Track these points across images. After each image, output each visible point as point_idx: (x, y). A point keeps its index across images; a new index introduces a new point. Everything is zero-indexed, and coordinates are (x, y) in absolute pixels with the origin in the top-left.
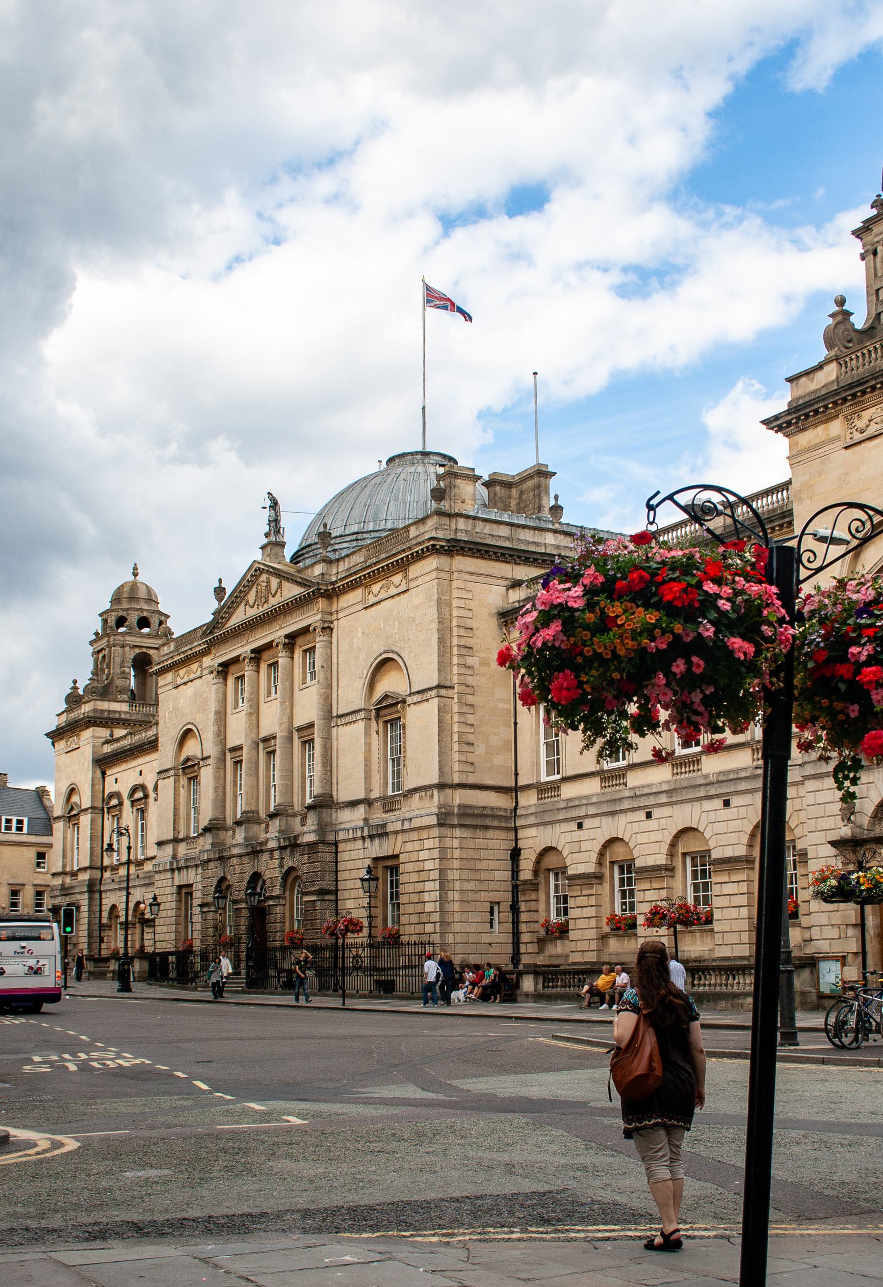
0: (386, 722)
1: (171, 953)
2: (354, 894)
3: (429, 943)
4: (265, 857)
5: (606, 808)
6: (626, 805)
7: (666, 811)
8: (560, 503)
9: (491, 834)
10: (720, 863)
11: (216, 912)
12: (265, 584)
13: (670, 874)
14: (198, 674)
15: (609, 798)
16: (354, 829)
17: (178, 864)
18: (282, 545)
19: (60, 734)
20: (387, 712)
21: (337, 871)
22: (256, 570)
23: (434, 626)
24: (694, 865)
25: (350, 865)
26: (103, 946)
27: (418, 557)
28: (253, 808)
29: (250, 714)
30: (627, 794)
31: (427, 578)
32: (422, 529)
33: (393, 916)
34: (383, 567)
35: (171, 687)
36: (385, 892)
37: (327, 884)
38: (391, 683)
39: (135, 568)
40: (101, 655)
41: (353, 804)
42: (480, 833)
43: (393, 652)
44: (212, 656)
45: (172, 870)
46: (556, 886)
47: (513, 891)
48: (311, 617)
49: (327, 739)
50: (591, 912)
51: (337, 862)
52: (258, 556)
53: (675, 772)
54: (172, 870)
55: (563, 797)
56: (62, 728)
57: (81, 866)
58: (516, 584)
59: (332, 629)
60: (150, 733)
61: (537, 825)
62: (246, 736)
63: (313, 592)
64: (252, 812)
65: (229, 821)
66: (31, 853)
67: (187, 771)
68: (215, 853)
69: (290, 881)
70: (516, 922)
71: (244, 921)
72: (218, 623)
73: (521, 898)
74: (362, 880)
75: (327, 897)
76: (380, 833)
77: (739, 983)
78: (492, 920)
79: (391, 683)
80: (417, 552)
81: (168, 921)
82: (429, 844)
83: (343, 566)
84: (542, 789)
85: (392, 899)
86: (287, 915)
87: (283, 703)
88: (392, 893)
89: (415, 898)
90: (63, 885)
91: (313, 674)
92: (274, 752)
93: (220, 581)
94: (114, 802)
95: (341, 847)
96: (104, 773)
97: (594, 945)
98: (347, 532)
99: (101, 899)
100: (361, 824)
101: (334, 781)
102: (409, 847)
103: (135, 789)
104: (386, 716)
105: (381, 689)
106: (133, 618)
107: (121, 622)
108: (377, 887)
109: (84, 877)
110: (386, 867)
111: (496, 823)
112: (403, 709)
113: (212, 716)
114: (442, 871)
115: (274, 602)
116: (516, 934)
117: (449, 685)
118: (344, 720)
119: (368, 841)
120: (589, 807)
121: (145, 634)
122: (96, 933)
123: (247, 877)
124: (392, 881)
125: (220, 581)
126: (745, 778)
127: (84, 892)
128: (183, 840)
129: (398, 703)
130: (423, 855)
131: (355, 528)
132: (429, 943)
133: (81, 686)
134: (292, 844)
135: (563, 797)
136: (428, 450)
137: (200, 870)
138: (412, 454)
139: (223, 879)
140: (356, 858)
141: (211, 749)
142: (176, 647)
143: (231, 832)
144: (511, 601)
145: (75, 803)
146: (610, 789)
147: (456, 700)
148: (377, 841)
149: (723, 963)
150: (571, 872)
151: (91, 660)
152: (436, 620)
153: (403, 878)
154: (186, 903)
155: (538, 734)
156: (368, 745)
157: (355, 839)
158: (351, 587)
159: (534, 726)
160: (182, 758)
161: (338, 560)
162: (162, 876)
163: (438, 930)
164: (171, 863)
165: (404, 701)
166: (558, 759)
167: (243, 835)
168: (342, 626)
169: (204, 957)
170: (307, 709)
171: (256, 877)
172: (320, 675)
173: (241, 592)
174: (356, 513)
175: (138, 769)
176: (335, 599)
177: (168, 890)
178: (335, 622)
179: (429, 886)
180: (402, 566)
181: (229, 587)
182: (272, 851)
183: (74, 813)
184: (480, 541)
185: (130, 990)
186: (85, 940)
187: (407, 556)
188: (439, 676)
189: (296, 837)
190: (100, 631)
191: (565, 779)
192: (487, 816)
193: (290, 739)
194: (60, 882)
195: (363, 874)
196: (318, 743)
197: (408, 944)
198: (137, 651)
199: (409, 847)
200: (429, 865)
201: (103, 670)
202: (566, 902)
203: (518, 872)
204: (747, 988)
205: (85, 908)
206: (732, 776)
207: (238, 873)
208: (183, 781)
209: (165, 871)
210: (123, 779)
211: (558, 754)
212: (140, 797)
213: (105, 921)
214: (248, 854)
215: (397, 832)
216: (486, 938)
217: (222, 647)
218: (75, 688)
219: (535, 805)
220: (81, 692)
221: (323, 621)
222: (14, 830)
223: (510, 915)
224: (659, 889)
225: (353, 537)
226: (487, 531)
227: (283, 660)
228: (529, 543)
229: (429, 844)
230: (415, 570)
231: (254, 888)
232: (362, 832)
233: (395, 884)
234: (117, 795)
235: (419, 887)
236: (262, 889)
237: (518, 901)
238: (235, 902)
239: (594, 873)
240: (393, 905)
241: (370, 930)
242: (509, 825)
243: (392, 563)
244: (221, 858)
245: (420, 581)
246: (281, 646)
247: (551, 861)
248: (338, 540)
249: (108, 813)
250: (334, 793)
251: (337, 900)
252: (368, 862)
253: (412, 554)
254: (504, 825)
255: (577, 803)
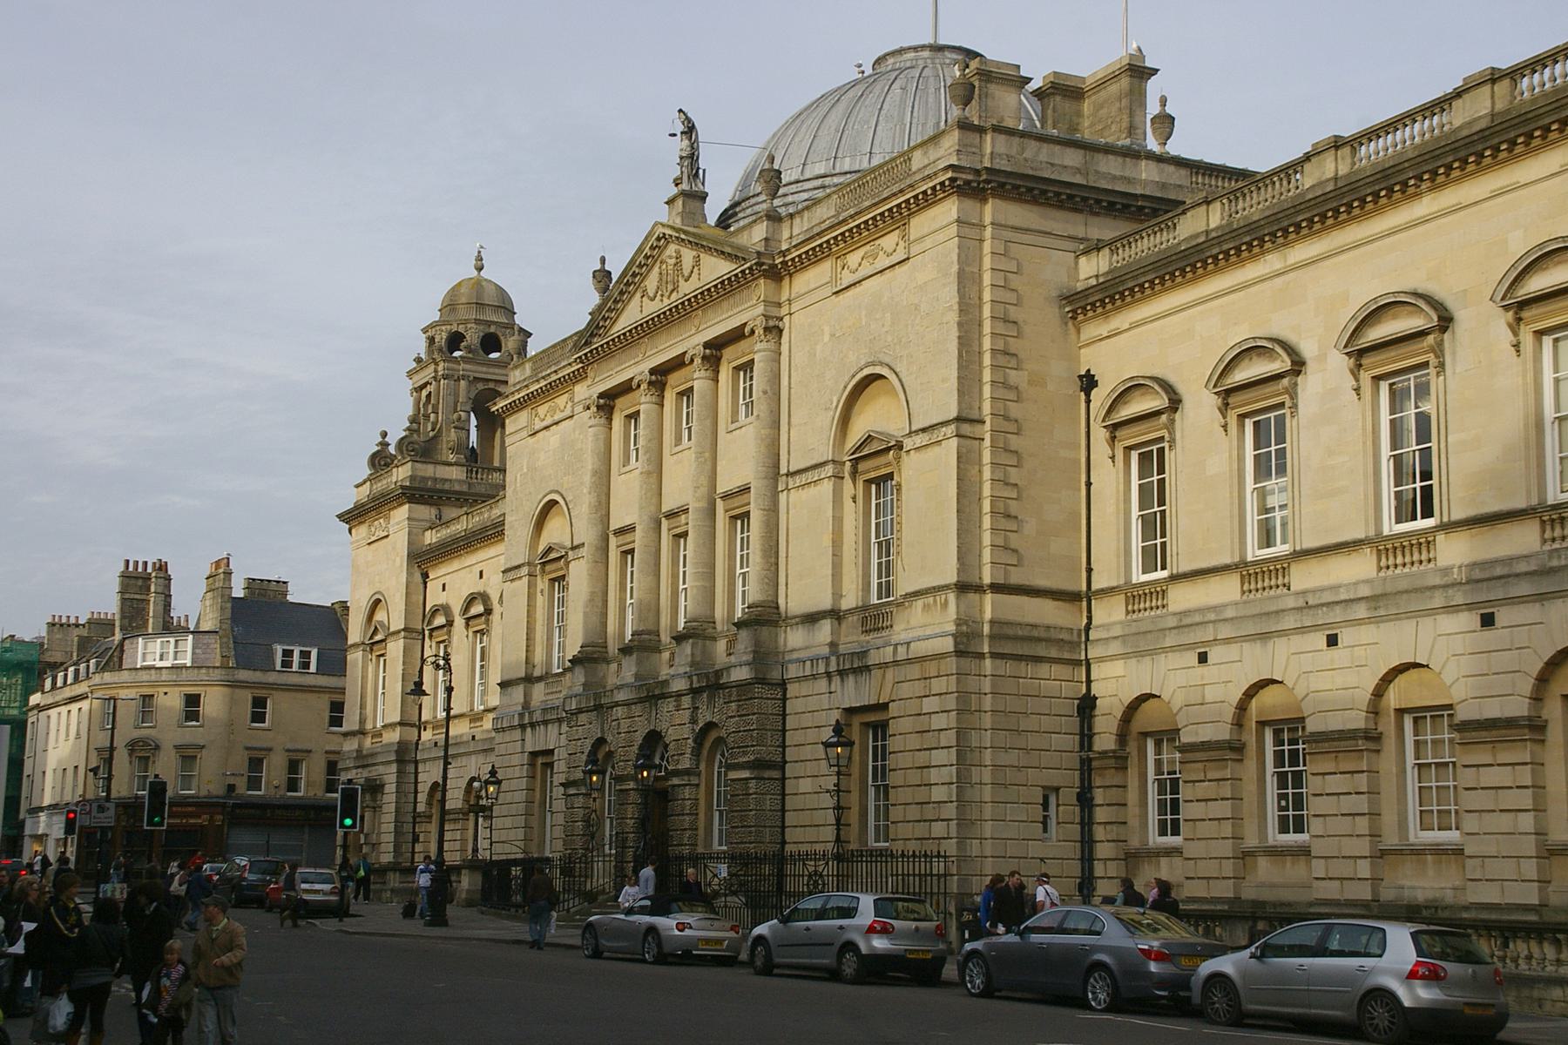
0: (869, 482)
1: (515, 862)
2: (810, 768)
3: (939, 856)
4: (667, 706)
5: (1251, 628)
6: (1289, 622)
7: (1367, 633)
8: (1169, 110)
9: (1044, 670)
10: (1475, 729)
11: (587, 795)
12: (673, 261)
13: (1372, 746)
14: (568, 412)
15: (1257, 611)
16: (814, 660)
17: (531, 717)
18: (703, 197)
19: (360, 515)
20: (871, 467)
21: (784, 731)
22: (659, 239)
23: (953, 317)
24: (1279, 742)
25: (807, 720)
26: (418, 847)
27: (925, 201)
28: (651, 627)
29: (649, 473)
30: (1291, 603)
31: (941, 237)
32: (933, 153)
33: (877, 808)
34: (866, 222)
35: (524, 433)
36: (864, 764)
37: (768, 752)
38: (875, 417)
39: (479, 258)
40: (424, 393)
41: (812, 619)
42: (1029, 669)
43: (881, 364)
44: (589, 381)
45: (523, 727)
46: (1158, 763)
47: (1081, 769)
48: (746, 311)
49: (773, 510)
50: (1224, 809)
51: (784, 715)
52: (663, 214)
53: (1548, 535)
54: (523, 727)
55: (1172, 608)
56: (363, 505)
57: (388, 721)
58: (1113, 245)
59: (781, 331)
60: (496, 512)
61: (1125, 656)
62: (641, 508)
63: (750, 268)
64: (649, 633)
65: (613, 648)
66: (323, 704)
67: (548, 568)
68: (588, 699)
69: (707, 745)
70: (1087, 823)
71: (631, 811)
72: (598, 327)
73: (1097, 781)
74: (827, 745)
75: (767, 774)
76: (856, 666)
77: (1529, 958)
78: (1045, 817)
79: (875, 417)
80: (924, 192)
81: (514, 809)
82: (938, 685)
83: (800, 227)
84: (1135, 596)
85: (875, 778)
86: (702, 803)
87: (699, 454)
88: (875, 768)
89: (914, 777)
90: (359, 751)
91: (749, 406)
92: (685, 535)
93: (603, 260)
94: (440, 620)
95: (792, 689)
96: (425, 576)
97: (1228, 868)
98: (807, 176)
99: (416, 773)
100: (826, 650)
101: (782, 580)
102: (906, 690)
103: (471, 600)
104: (868, 471)
105: (861, 426)
106: (473, 336)
107: (455, 340)
108: (850, 758)
109: (393, 737)
110: (867, 725)
111: (1054, 653)
112: (898, 459)
113: (587, 479)
114: (961, 733)
115: (687, 288)
116: (1087, 842)
117: (976, 417)
118: (799, 480)
119: (836, 680)
120: (1221, 626)
121: (494, 360)
122: (408, 827)
123: (639, 738)
124: (875, 748)
125: (603, 260)
126: (1526, 574)
127: (390, 762)
128: (540, 679)
129: (889, 449)
130: (930, 705)
131: (820, 169)
132: (939, 856)
133: (393, 440)
134: (710, 684)
135: (1172, 608)
136: (942, 41)
137: (565, 728)
138: (915, 49)
139: (601, 741)
140: (815, 707)
141: (586, 533)
142: (533, 370)
143: (614, 666)
144: (1082, 276)
145: (381, 623)
146: (1259, 595)
147: (987, 443)
148: (851, 678)
149: (1484, 916)
150: (1186, 738)
151: (410, 401)
152: (956, 307)
153: (894, 744)
154: (544, 781)
155: (1127, 500)
156: (838, 521)
157: (814, 677)
158: (813, 258)
159: (1121, 487)
160: (541, 548)
161: (791, 216)
162: (507, 736)
163: (953, 833)
164: (521, 715)
165: (899, 446)
166: (1164, 545)
167: (634, 670)
168: (796, 326)
169: (567, 871)
170: (739, 464)
171: (654, 739)
172: (761, 407)
173: (634, 275)
174: (823, 143)
175: (477, 569)
176: (787, 279)
177: (516, 760)
178: (786, 319)
179: (938, 757)
180: (898, 217)
181: (616, 268)
182: (679, 695)
183: (378, 638)
184: (1031, 172)
185: (444, 923)
186: (391, 838)
187: (907, 201)
188: (959, 403)
189: (718, 674)
190: (423, 356)
191: (1174, 578)
192: (1039, 640)
193: (711, 512)
194: (356, 746)
195: (827, 734)
196: (756, 518)
197: (903, 855)
198: (480, 386)
199: (906, 690)
200: (939, 722)
201: (427, 417)
202: (1175, 791)
203: (1091, 737)
204: (1549, 968)
205: (391, 788)
206: (1499, 571)
207: (626, 731)
208: (542, 584)
209: (512, 728)
210: (453, 583)
211: (1163, 535)
212: (479, 609)
213: (421, 808)
214: (641, 701)
215: (884, 666)
216: (1035, 849)
217: (604, 365)
218: (385, 445)
219: (1121, 623)
220: (392, 450)
221: (767, 317)
222: (295, 667)
223: (1077, 809)
224: (1352, 772)
225: (818, 182)
226: (1043, 157)
227: (700, 384)
228: (1114, 177)
229: (938, 685)
230: (920, 224)
231: (649, 757)
232: (827, 665)
233: (881, 753)
234: (445, 609)
235: (922, 758)
236: (662, 759)
237: (1090, 788)
238: (619, 779)
239: (1228, 742)
240: (877, 788)
241: (838, 830)
242: (1075, 657)
243: (882, 214)
244: (598, 708)
245: (928, 243)
246: (698, 361)
247: (1147, 717)
248: (793, 188)
249: (431, 637)
250: (781, 601)
251: (784, 779)
252: (836, 715)
253: (915, 197)
254: (1066, 656)
255: (1197, 618)
